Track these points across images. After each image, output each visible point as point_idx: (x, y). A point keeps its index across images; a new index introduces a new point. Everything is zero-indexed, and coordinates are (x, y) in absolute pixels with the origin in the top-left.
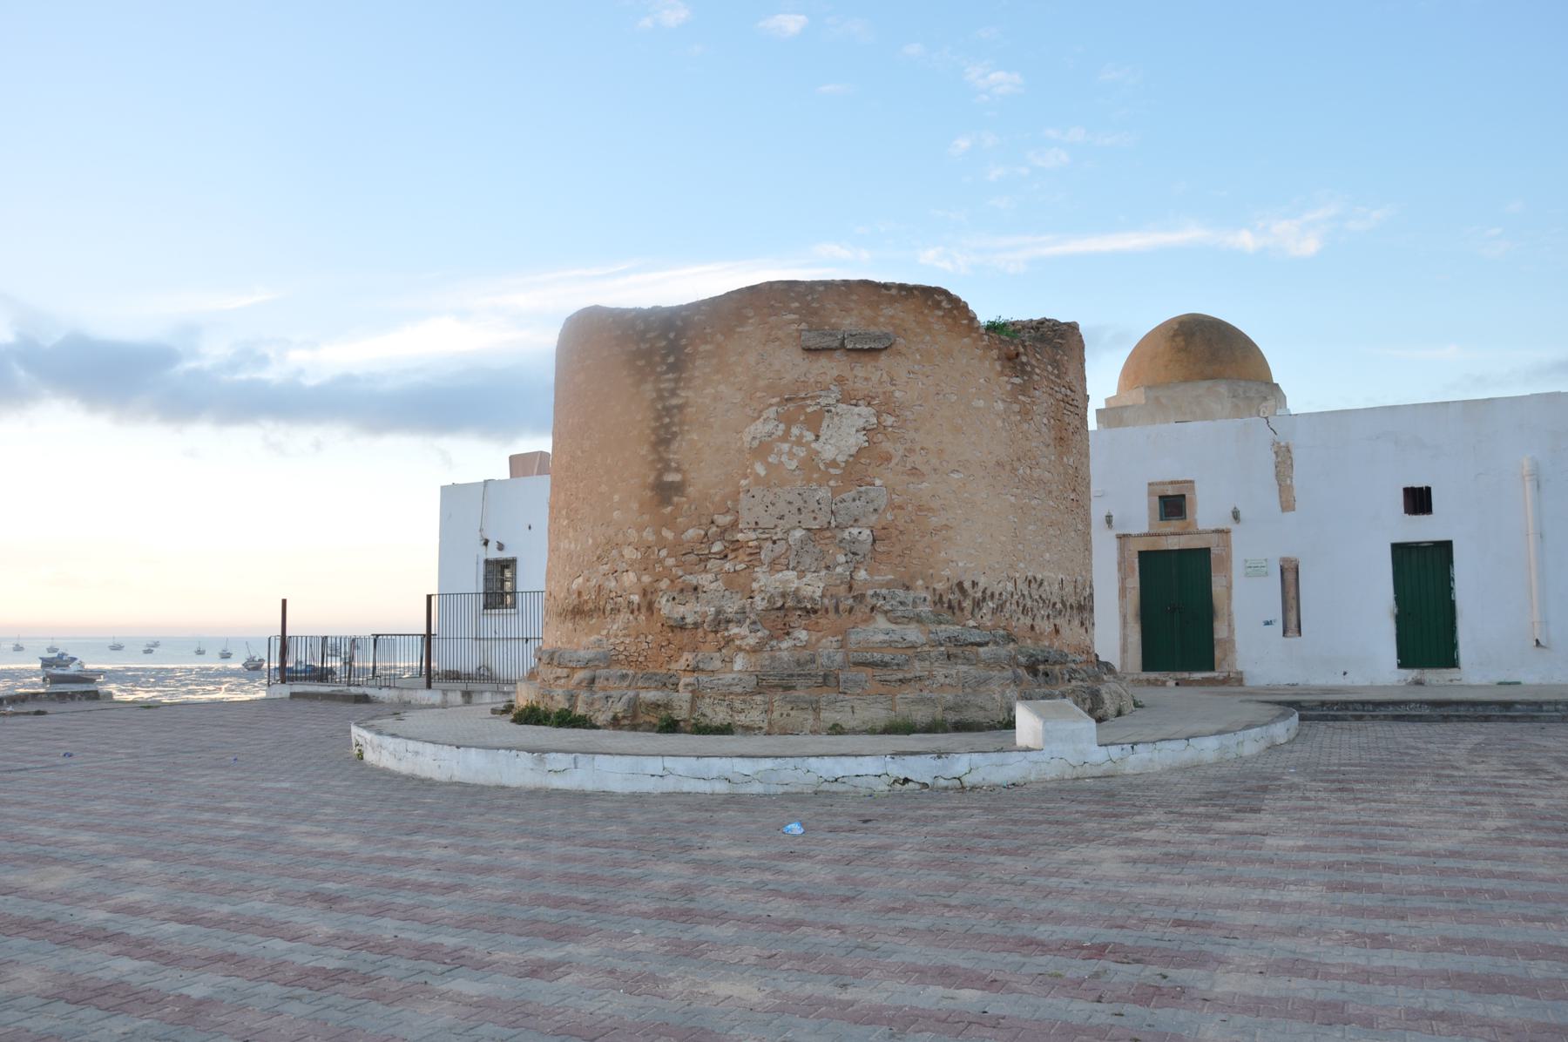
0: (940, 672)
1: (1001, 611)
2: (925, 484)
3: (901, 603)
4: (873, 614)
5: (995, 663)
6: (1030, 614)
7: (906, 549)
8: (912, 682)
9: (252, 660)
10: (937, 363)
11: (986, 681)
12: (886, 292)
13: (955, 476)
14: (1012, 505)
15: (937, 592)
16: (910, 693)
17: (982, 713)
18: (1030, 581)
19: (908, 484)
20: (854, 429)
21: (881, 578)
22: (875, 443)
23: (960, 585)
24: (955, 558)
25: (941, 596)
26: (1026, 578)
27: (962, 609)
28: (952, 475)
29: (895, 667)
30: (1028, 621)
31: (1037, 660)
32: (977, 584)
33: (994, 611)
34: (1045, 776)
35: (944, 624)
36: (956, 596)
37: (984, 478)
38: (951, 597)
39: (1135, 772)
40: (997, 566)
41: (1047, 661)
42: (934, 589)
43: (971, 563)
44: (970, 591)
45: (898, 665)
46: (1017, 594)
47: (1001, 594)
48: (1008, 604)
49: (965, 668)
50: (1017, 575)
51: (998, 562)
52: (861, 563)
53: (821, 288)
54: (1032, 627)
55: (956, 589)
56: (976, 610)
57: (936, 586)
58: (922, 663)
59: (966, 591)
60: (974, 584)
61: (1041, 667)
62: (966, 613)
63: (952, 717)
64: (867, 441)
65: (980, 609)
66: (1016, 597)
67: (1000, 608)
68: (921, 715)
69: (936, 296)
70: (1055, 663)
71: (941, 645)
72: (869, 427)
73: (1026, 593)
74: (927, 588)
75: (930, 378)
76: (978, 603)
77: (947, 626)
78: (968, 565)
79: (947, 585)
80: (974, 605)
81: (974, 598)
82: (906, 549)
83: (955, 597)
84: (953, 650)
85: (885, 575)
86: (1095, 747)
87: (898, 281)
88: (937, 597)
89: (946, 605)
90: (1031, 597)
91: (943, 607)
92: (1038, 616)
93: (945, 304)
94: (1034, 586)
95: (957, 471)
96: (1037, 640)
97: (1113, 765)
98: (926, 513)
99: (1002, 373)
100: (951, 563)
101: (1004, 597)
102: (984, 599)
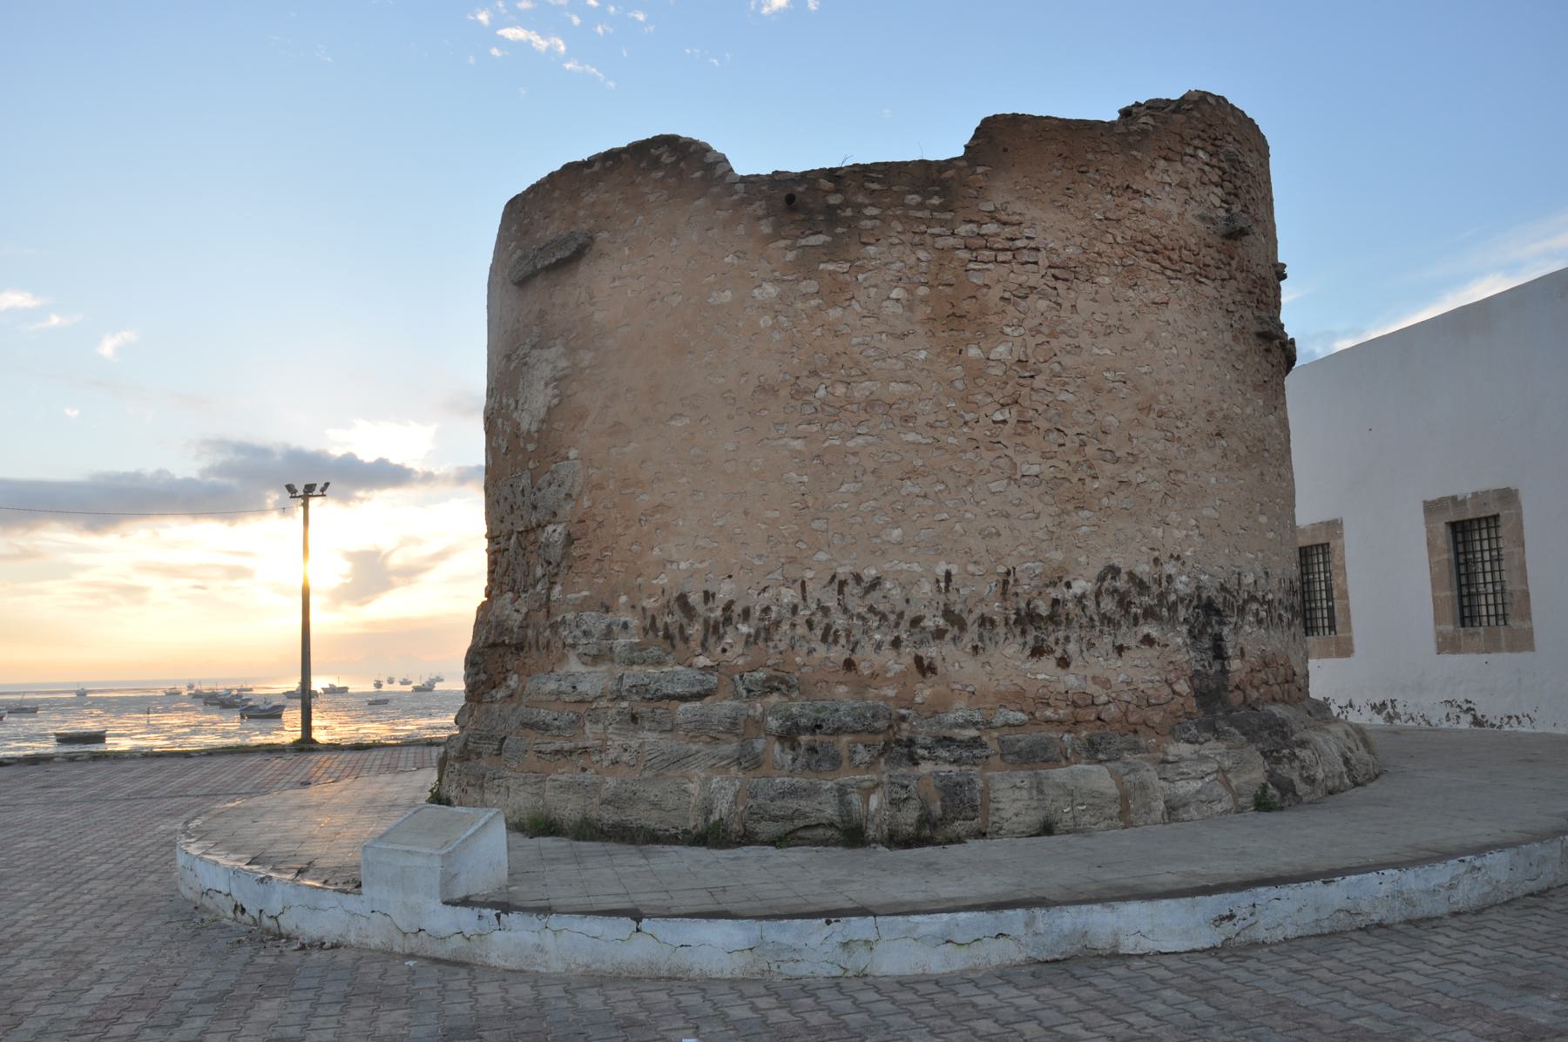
0: (616, 741)
1: (766, 640)
2: (633, 445)
3: (585, 633)
4: (565, 651)
5: (700, 728)
6: (843, 641)
7: (606, 548)
8: (574, 757)
9: (1059, 665)
10: (651, 253)
11: (680, 760)
12: (589, 171)
13: (677, 423)
14: (796, 454)
15: (649, 614)
16: (564, 774)
17: (655, 814)
18: (842, 584)
19: (609, 448)
20: (543, 383)
21: (574, 596)
22: (569, 396)
23: (682, 600)
24: (675, 557)
25: (653, 618)
26: (834, 577)
27: (686, 639)
28: (673, 423)
29: (555, 732)
30: (838, 653)
31: (796, 725)
32: (713, 595)
33: (750, 641)
34: (368, 941)
35: (638, 664)
36: (676, 617)
37: (730, 417)
38: (668, 619)
39: (508, 965)
40: (757, 562)
41: (819, 727)
42: (644, 609)
43: (702, 562)
44: (701, 609)
45: (559, 728)
46: (807, 607)
47: (767, 610)
48: (785, 627)
49: (651, 737)
50: (809, 574)
51: (760, 556)
52: (556, 574)
53: (531, 195)
54: (849, 665)
55: (676, 607)
56: (712, 640)
57: (644, 604)
58: (595, 726)
59: (693, 609)
60: (708, 596)
61: (804, 739)
62: (692, 644)
63: (609, 816)
64: (557, 396)
65: (720, 638)
66: (804, 613)
67: (766, 633)
68: (569, 808)
69: (653, 151)
70: (837, 731)
71: (623, 699)
72: (558, 376)
73: (832, 604)
74: (633, 607)
75: (643, 278)
76: (716, 628)
77: (643, 667)
78: (698, 565)
79: (662, 601)
80: (707, 630)
81: (706, 622)
82: (606, 548)
83: (674, 619)
84: (643, 708)
85: (580, 591)
86: (435, 904)
87: (603, 149)
88: (648, 622)
89: (661, 633)
90: (845, 610)
91: (657, 636)
92: (864, 641)
93: (667, 159)
94: (852, 589)
95: (681, 415)
96: (861, 687)
97: (464, 943)
98: (632, 490)
99: (776, 236)
100: (669, 566)
101: (773, 615)
102: (728, 620)
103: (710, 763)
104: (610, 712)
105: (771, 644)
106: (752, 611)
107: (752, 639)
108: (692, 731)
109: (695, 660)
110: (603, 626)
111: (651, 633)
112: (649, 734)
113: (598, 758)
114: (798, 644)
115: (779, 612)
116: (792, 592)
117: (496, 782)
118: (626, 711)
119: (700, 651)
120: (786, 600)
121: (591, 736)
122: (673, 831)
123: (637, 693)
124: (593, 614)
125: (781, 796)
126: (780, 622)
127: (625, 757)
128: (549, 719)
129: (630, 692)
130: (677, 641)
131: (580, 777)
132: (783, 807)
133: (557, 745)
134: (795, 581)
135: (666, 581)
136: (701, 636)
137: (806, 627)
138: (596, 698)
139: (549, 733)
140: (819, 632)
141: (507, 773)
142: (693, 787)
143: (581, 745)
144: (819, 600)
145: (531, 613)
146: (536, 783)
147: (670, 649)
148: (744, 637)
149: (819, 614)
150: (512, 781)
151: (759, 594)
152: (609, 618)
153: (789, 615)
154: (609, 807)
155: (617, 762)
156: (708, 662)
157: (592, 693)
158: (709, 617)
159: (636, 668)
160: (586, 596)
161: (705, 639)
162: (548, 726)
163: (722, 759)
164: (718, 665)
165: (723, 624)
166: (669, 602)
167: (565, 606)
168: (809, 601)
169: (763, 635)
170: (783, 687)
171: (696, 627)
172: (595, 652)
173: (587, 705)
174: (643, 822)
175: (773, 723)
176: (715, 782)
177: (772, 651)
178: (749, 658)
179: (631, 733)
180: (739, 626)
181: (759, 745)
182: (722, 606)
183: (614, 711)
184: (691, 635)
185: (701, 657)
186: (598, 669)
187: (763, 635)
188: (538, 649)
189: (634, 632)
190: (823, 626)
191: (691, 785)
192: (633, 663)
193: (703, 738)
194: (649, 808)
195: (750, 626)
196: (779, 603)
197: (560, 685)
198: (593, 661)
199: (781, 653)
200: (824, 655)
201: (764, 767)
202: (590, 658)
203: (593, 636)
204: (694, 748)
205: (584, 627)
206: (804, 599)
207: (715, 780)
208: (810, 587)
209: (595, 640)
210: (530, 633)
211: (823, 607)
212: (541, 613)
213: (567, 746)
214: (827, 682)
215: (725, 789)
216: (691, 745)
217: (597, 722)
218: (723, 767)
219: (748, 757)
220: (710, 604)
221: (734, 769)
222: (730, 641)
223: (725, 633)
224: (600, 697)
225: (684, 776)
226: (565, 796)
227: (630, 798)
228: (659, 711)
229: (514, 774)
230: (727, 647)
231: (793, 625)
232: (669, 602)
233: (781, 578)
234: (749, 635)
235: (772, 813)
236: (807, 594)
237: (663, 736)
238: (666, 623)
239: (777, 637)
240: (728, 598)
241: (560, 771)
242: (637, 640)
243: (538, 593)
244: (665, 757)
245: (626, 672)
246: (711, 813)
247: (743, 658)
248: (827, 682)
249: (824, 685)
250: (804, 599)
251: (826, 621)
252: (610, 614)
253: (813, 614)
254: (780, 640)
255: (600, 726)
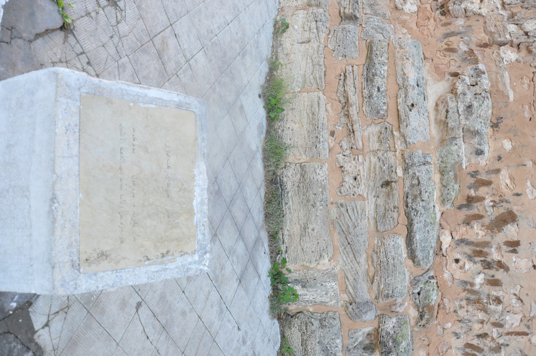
1: (468, 299)
4: (447, 76)
8: (344, 120)
17: (296, 229)
21: (508, 81)
25: (488, 183)
27: (467, 222)
32: (514, 251)
35: (442, 180)
36: (490, 210)
38: (488, 202)
42: (498, 171)
44: (500, 238)
47: (498, 301)
48: (481, 315)
49: (370, 208)
55: (502, 211)
56: (468, 249)
65: (470, 258)
66: (494, 332)
71: (406, 170)
74: (500, 158)
76: (480, 253)
77: (438, 185)
79: (508, 194)
80: (478, 245)
81: (487, 244)
85: (513, 88)
88: (484, 177)
89: (472, 193)
91: (470, 188)
101: (493, 307)
103: (349, 275)
104: (390, 154)
105: (464, 303)
106: (497, 288)
107: (468, 287)
108: (378, 258)
109: (447, 233)
110: (478, 127)
111: (472, 180)
112: (373, 206)
113: (345, 146)
114: (464, 325)
115: (495, 312)
116: (517, 324)
117: (313, 25)
118: (393, 175)
119: (456, 238)
120: (508, 318)
121: (366, 134)
122: (283, 248)
123: (412, 186)
124: (490, 112)
125: (325, 348)
126: (486, 312)
127: (349, 180)
128: (378, 81)
129: (413, 177)
130: (465, 212)
131: (325, 134)
132: (315, 351)
133: (354, 99)
134: (528, 327)
135: (530, 197)
136: (472, 238)
137: (481, 332)
138: (403, 136)
139: (365, 84)
140: (475, 342)
141: (323, 35)
142: (325, 264)
143: (356, 127)
144: (508, 345)
145: (481, 20)
146: (315, 78)
147: (457, 204)
148: (471, 280)
149: (493, 345)
150: (315, 46)
151: (515, 295)
152: (487, 131)
153: (492, 320)
154: (298, 176)
155: (343, 171)
156: (444, 247)
157: (408, 132)
158: (491, 247)
159: (437, 177)
160: (508, 97)
161: (468, 243)
162: (372, 81)
163: (354, 288)
164: (443, 255)
165: (484, 261)
166: (507, 202)
167: (494, 69)
168: (507, 337)
169: (473, 297)
170: (423, 322)
171: (480, 232)
172: (451, 124)
173: (395, 124)
174: (288, 216)
175: (390, 324)
176: (333, 285)
177: (457, 303)
178: (450, 284)
179: (372, 184)
180: (482, 276)
181: (370, 316)
182: (503, 260)
183: (392, 160)
184: (472, 227)
185: (450, 238)
186: (433, 125)
187: (473, 297)
188: (447, 35)
189: (473, 161)
190: (481, 346)
191: (326, 261)
192: (442, 173)
193: (372, 268)
194: (301, 222)
195: (482, 285)
196: (505, 313)
197: (414, 88)
198: (441, 121)
199: (455, 311)
200: (454, 346)
201: (350, 322)
202: (443, 118)
203: (467, 119)
204: (362, 259)
205: (475, 104)
206: (508, 334)
207: (333, 284)
208: (522, 340)
209: (463, 122)
210: (461, 22)
211: (500, 348)
212: (483, 35)
213: (353, 111)
214: (429, 345)
215: (326, 294)
216: (364, 256)
217: (380, 141)
218: (347, 287)
219: (357, 311)
220: (504, 248)
221: (345, 297)
222: (467, 267)
223: (475, 263)
224: (406, 141)
225: (335, 249)
226: (305, 120)
227: (308, 201)
228: (395, 215)
229: (322, 46)
230: (461, 263)
231: (482, 322)
232: (507, 202)
233: (532, 315)
234: (472, 285)
235: (309, 343)
236: (513, 337)
237: (372, 222)
238: (484, 199)
239: (470, 308)
240: (511, 266)
241: (329, 108)
242: (464, 167)
243: (505, 29)
244: (351, 230)
245: (432, 168)
246: (304, 287)
247: (451, 279)
248: (429, 345)
249: (426, 343)
250: (508, 334)
251: (486, 349)
252: (490, 130)
253: (493, 339)
254: (467, 311)
255: (376, 146)
